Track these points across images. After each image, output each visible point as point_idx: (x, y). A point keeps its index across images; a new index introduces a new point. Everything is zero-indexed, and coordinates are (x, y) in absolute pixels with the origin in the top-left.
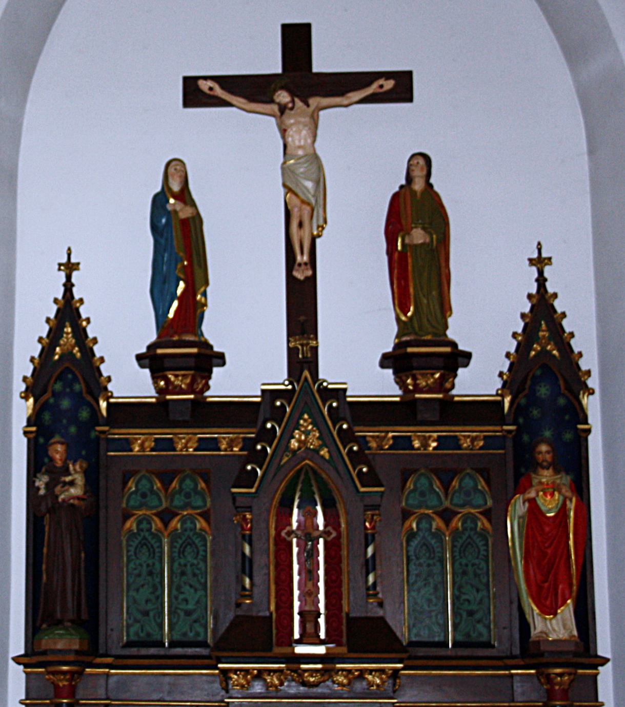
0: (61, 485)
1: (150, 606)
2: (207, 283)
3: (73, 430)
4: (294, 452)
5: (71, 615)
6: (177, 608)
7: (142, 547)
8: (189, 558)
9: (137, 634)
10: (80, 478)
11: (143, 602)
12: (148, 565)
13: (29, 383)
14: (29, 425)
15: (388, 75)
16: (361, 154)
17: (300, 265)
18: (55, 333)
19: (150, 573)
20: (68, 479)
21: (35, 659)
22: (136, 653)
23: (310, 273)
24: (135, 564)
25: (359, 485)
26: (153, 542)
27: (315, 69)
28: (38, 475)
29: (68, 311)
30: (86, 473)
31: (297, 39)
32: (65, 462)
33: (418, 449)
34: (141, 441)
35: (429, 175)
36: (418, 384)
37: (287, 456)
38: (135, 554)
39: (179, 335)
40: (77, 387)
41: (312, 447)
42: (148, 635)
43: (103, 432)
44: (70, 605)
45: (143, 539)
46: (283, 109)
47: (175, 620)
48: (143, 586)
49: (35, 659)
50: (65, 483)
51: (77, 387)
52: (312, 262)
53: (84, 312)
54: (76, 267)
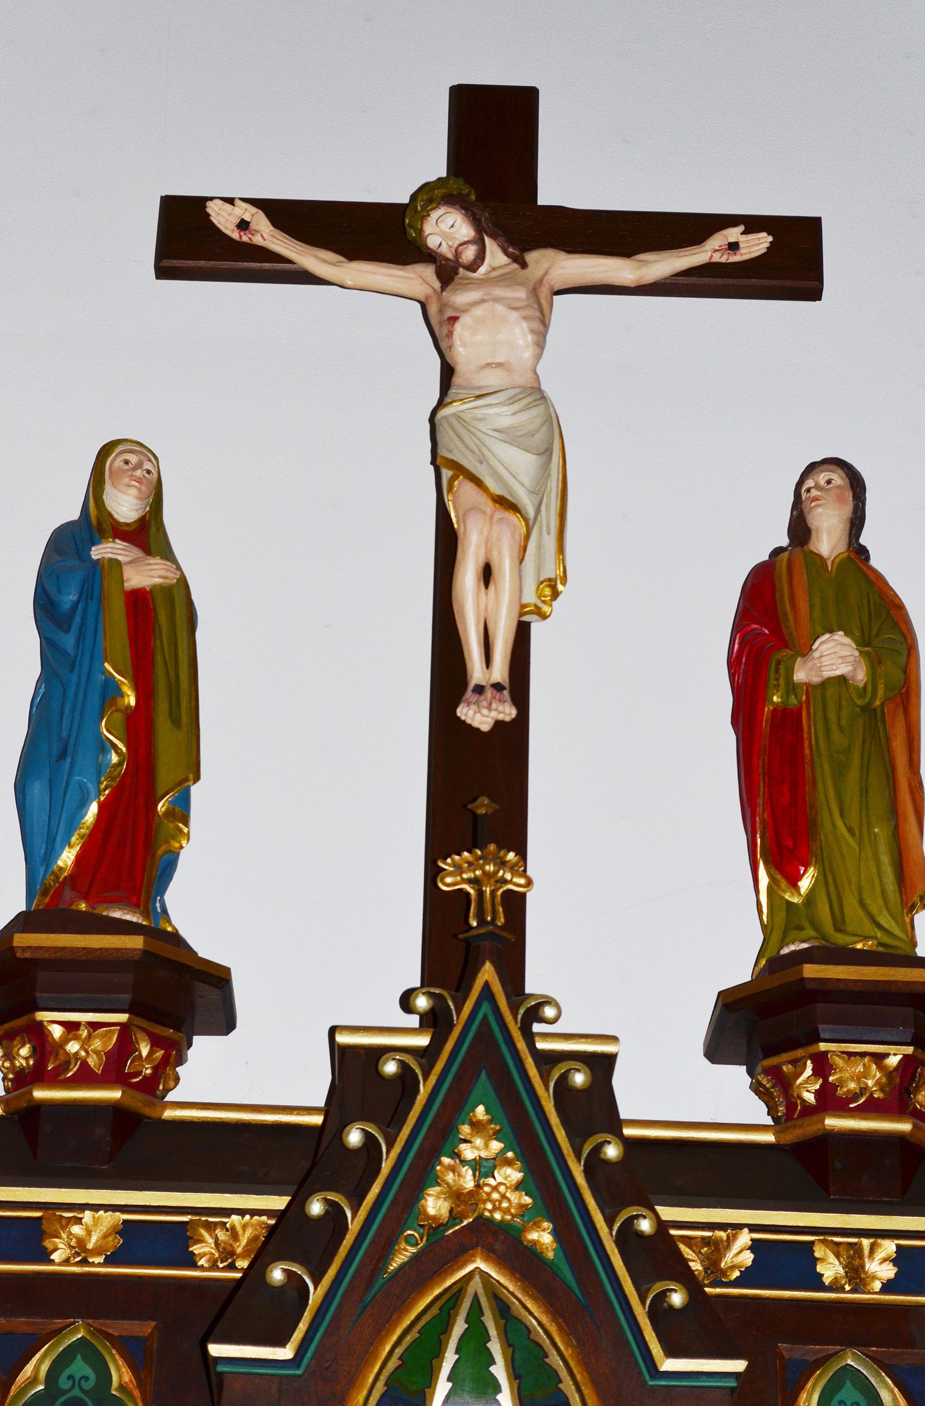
4: (435, 1228)
15: (753, 224)
16: (670, 458)
17: (479, 689)
23: (508, 712)
25: (656, 1348)
27: (544, 199)
31: (493, 133)
33: (835, 1287)
35: (857, 522)
36: (834, 1087)
37: (409, 1240)
41: (498, 1216)
46: (448, 272)
52: (518, 685)
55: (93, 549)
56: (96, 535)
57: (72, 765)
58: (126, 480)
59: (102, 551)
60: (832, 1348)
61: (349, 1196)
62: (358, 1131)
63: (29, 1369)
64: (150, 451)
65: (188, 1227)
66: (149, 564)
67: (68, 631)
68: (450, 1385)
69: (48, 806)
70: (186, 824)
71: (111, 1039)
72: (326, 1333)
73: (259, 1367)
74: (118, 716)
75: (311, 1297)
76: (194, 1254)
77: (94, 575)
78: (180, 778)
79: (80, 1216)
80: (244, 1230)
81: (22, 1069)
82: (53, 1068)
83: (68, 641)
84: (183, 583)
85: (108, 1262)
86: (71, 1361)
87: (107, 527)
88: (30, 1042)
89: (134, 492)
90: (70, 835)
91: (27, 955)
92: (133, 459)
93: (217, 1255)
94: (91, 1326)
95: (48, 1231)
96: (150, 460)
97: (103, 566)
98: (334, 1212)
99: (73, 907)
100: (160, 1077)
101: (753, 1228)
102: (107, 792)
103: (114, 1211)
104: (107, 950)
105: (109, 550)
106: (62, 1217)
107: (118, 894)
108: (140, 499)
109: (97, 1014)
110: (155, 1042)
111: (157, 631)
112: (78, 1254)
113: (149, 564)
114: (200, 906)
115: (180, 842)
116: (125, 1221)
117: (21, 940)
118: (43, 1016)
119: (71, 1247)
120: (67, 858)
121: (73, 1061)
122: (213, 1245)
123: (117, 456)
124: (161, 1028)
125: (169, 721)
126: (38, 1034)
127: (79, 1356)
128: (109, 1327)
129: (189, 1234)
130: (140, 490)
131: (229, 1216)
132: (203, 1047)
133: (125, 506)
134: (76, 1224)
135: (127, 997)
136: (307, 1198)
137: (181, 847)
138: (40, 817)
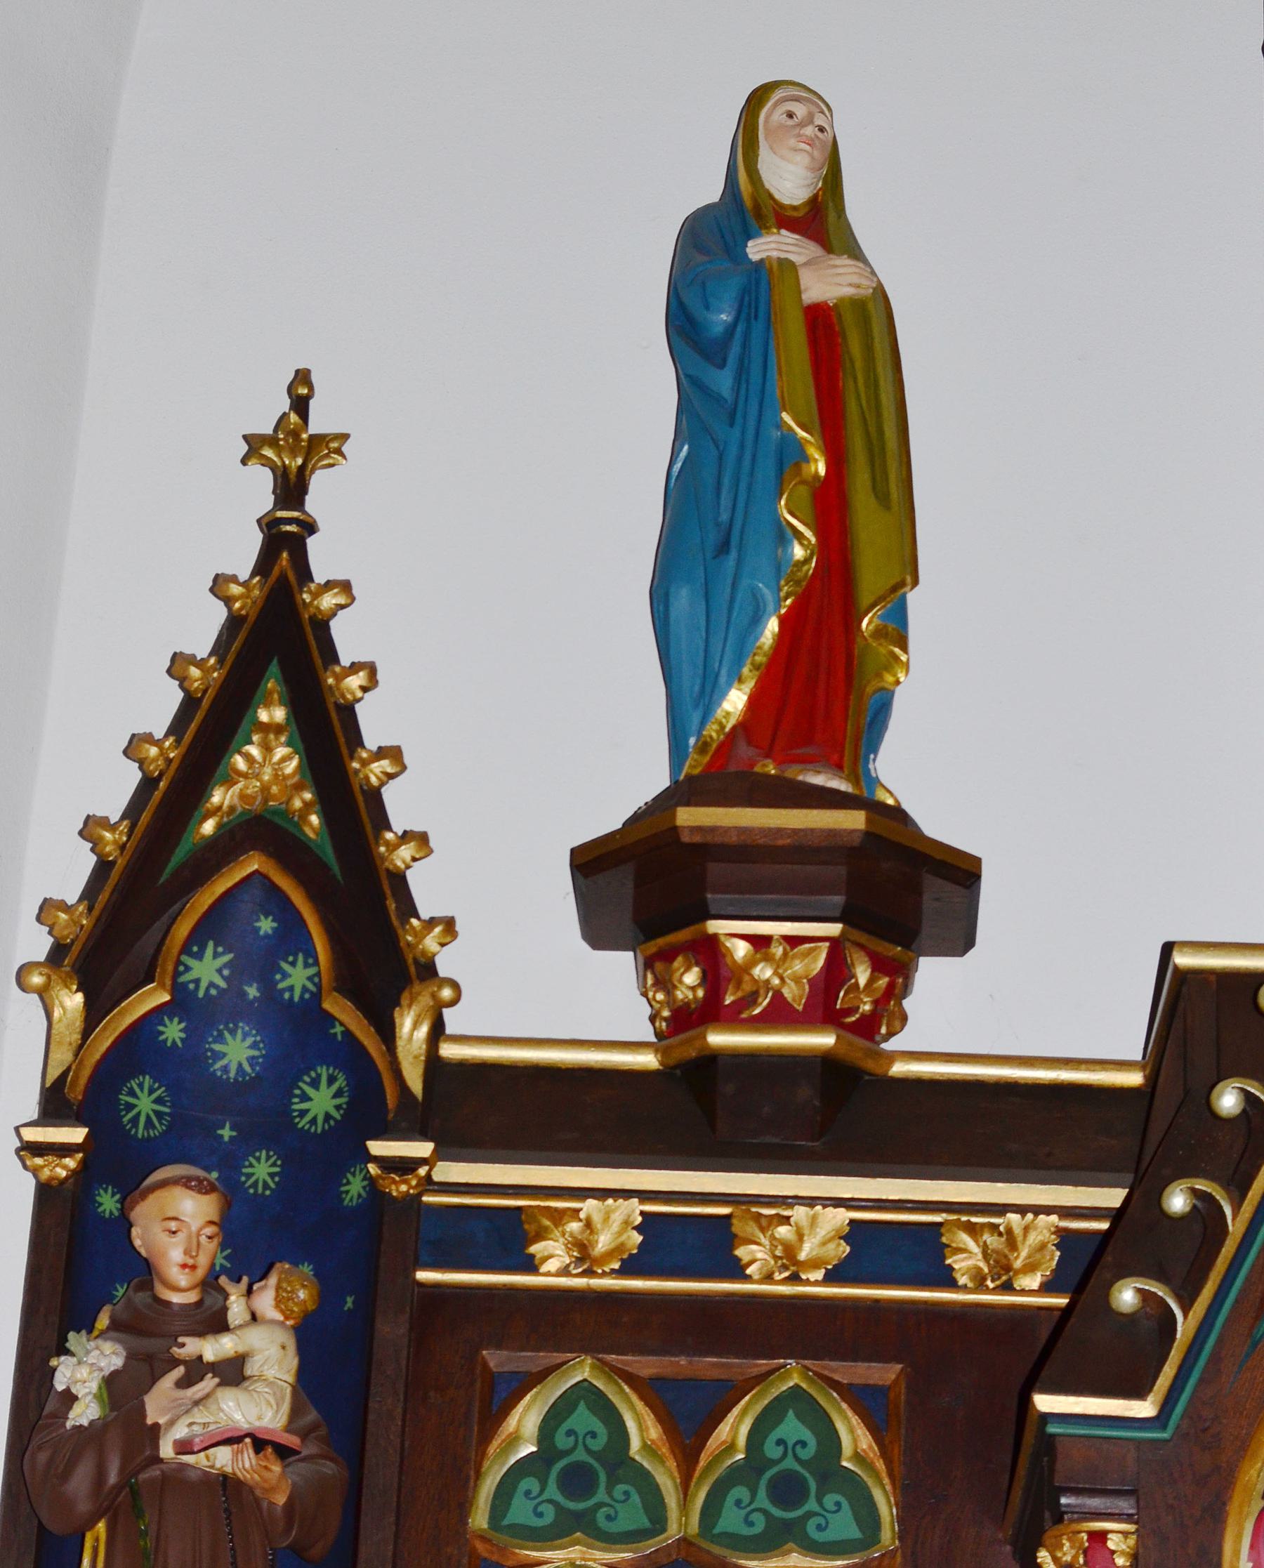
0: (180, 1371)
2: (910, 572)
3: (261, 1170)
10: (273, 1351)
13: (68, 934)
14: (55, 1104)
18: (209, 725)
20: (213, 1349)
29: (278, 640)
30: (310, 1336)
32: (210, 1284)
34: (593, 1219)
39: (779, 763)
40: (296, 978)
43: (405, 1166)
50: (196, 1370)
51: (296, 978)
53: (349, 636)
54: (325, 448)
55: (750, 244)
56: (753, 222)
57: (739, 562)
58: (792, 142)
59: (757, 249)
60: (558, 1357)
61: (1226, 1185)
62: (1235, 1091)
63: (723, 1431)
64: (815, 93)
65: (943, 1230)
66: (836, 266)
67: (722, 366)
69: (703, 623)
70: (905, 649)
71: (815, 960)
72: (1201, 1381)
73: (1111, 1427)
74: (804, 491)
75: (1179, 1328)
76: (953, 1269)
77: (758, 283)
78: (892, 582)
79: (786, 1213)
80: (1025, 1236)
81: (687, 1004)
82: (733, 1003)
83: (723, 381)
84: (880, 294)
85: (830, 1278)
86: (780, 1419)
87: (767, 211)
88: (697, 964)
89: (803, 159)
90: (739, 662)
91: (697, 839)
92: (800, 110)
93: (986, 1270)
95: (740, 1234)
96: (822, 112)
97: (771, 268)
98: (1206, 1211)
99: (758, 769)
100: (882, 1016)
101: (646, 1196)
102: (789, 602)
103: (836, 1206)
104: (812, 830)
105: (773, 246)
106: (760, 1215)
107: (809, 750)
108: (812, 170)
109: (797, 925)
110: (880, 965)
111: (848, 365)
112: (785, 1267)
113: (836, 266)
114: (928, 767)
115: (895, 675)
116: (852, 1222)
117: (687, 816)
118: (717, 927)
119: (776, 1258)
120: (735, 701)
121: (762, 992)
122: (980, 1256)
123: (776, 105)
124: (887, 945)
125: (872, 500)
126: (709, 953)
127: (791, 1413)
128: (834, 1371)
129: (944, 1240)
130: (813, 158)
131: (791, 1206)
132: (932, 974)
133: (789, 180)
134: (782, 1224)
135: (839, 899)
136: (1167, 1186)
137: (898, 683)
138: (687, 641)
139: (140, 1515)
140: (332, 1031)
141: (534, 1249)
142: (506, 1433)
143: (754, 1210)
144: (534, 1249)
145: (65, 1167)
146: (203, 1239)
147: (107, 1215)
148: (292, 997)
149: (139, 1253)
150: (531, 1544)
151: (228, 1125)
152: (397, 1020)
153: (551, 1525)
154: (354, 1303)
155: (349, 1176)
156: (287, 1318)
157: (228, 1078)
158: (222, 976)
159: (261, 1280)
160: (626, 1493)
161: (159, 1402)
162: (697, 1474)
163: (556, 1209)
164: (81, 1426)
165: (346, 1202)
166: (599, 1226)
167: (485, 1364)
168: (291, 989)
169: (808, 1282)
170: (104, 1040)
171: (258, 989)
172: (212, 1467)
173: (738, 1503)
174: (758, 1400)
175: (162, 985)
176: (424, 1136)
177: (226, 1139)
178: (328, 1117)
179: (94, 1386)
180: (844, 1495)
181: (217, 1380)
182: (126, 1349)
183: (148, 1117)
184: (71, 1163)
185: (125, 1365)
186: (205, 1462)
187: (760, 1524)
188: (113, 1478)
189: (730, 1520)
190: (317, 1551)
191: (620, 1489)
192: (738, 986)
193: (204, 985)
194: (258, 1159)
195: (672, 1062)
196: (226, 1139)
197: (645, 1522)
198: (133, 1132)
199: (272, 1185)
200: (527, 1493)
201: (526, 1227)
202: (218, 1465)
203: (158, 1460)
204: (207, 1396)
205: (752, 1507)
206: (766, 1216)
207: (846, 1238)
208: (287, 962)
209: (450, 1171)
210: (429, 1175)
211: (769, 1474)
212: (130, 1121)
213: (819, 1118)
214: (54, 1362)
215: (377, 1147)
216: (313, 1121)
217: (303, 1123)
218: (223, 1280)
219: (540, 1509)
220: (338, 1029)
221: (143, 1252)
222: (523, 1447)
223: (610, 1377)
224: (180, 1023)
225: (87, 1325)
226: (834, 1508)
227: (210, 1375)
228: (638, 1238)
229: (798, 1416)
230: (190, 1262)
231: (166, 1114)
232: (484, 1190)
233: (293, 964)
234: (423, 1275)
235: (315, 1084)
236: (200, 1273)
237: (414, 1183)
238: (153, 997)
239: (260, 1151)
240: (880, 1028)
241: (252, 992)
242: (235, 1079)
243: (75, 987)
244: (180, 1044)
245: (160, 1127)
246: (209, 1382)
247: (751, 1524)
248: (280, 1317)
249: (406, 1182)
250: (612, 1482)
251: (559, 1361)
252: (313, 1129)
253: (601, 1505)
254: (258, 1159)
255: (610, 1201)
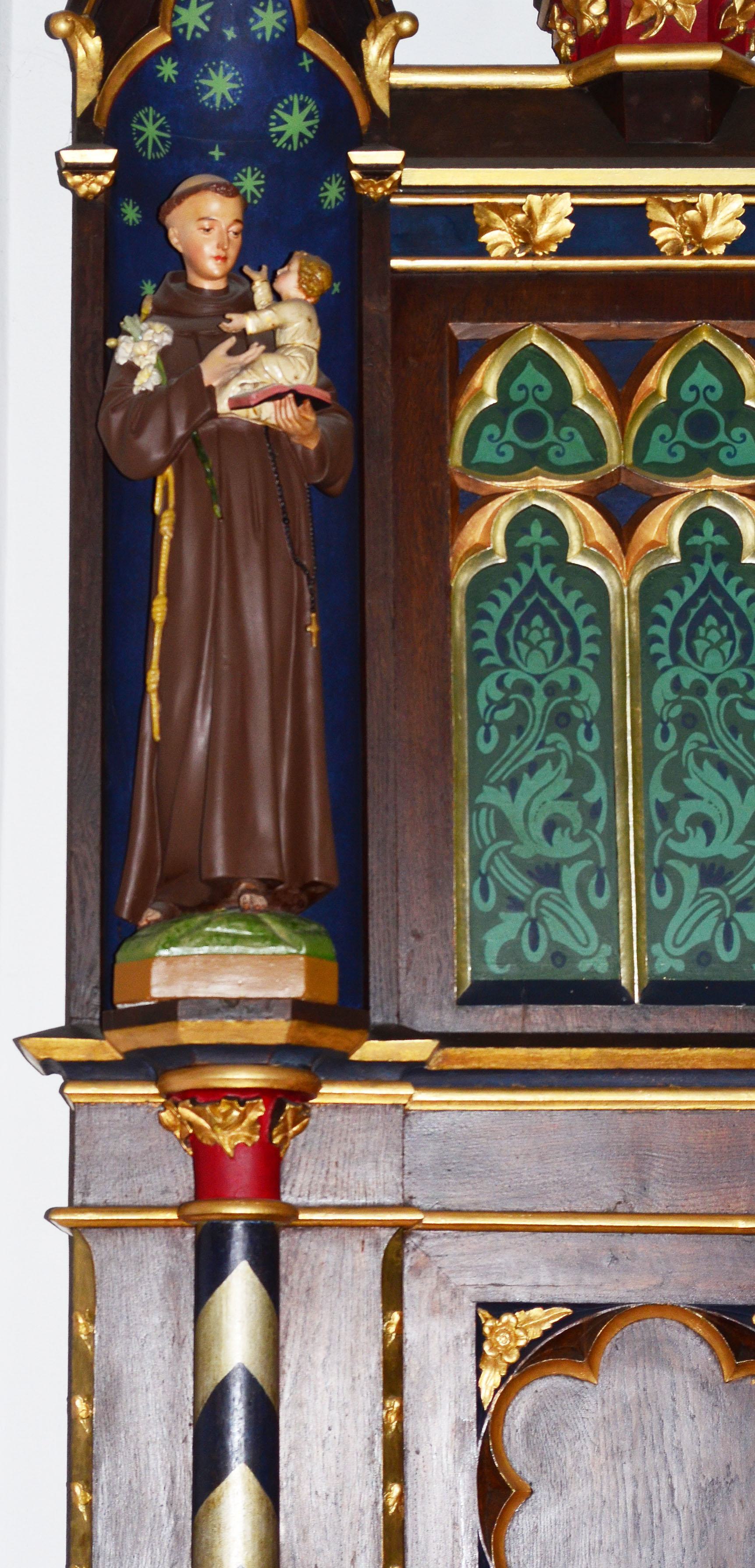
0: (231, 342)
1: (562, 846)
3: (250, 182)
5: (269, 862)
6: (668, 853)
7: (526, 620)
8: (713, 662)
9: (510, 952)
11: (537, 830)
12: (552, 690)
14: (85, 132)
19: (562, 720)
20: (251, 324)
21: (104, 1049)
22: (514, 1027)
24: (500, 684)
26: (568, 601)
28: (128, 323)
32: (236, 274)
34: (532, 211)
38: (502, 644)
42: (559, 955)
43: (381, 172)
44: (264, 821)
45: (527, 592)
47: (662, 903)
48: (533, 768)
49: (104, 1049)
50: (244, 341)
60: (511, 326)
63: (650, 381)
68: (206, 384)
81: (592, 31)
86: (692, 370)
94: (717, 327)
101: (576, 190)
119: (685, 237)
121: (659, 16)
127: (700, 364)
128: (738, 328)
131: (697, 194)
139: (205, 460)
140: (301, 64)
141: (484, 238)
142: (471, 392)
143: (664, 199)
144: (484, 238)
145: (99, 183)
146: (231, 234)
147: (131, 224)
148: (264, 37)
149: (176, 250)
150: (498, 477)
151: (217, 147)
152: (364, 51)
153: (511, 462)
154: (340, 287)
155: (326, 184)
156: (308, 296)
157: (215, 108)
158: (205, 22)
159: (283, 266)
160: (571, 434)
161: (214, 366)
162: (631, 415)
163: (501, 205)
164: (147, 391)
165: (325, 206)
166: (538, 217)
167: (451, 334)
168: (263, 30)
169: (711, 257)
170: (118, 78)
171: (235, 32)
172: (259, 420)
173: (662, 438)
174: (675, 355)
175: (164, 28)
176: (397, 146)
177: (217, 159)
178: (302, 137)
179: (153, 358)
180: (746, 427)
181: (263, 347)
182: (173, 328)
183: (154, 141)
184: (105, 179)
185: (174, 341)
186: (253, 416)
187: (681, 454)
188: (180, 432)
189: (657, 452)
190: (338, 486)
191: (565, 431)
192: (639, 11)
193: (190, 29)
194: (245, 175)
195: (582, 80)
196: (217, 159)
197: (587, 456)
198: (144, 154)
199: (259, 196)
200: (491, 437)
201: (478, 220)
202: (263, 418)
203: (214, 414)
204: (253, 362)
205: (675, 440)
206: (674, 204)
207: (743, 219)
208: (258, 7)
209: (414, 176)
210: (400, 179)
211: (686, 414)
212: (141, 145)
213: (709, 121)
214: (111, 342)
215: (358, 157)
216: (290, 141)
217: (281, 143)
218: (247, 269)
219: (502, 449)
220: (306, 62)
221: (180, 248)
222: (486, 400)
223: (553, 340)
224: (173, 62)
225: (135, 310)
226: (740, 439)
227: (256, 344)
228: (570, 226)
229: (706, 367)
230: (223, 254)
231: (168, 139)
232: (440, 191)
233: (264, 9)
234: (397, 263)
235: (288, 110)
236: (230, 262)
237: (389, 185)
238: (157, 39)
239: (246, 167)
240: (749, 46)
241: (230, 34)
242: (221, 109)
243: (94, 32)
244: (174, 81)
245: (164, 151)
246: (256, 350)
247: (674, 455)
248: (302, 296)
249: (382, 185)
250: (559, 424)
251: (511, 329)
252: (290, 148)
253: (551, 444)
254: (245, 175)
255: (547, 196)
